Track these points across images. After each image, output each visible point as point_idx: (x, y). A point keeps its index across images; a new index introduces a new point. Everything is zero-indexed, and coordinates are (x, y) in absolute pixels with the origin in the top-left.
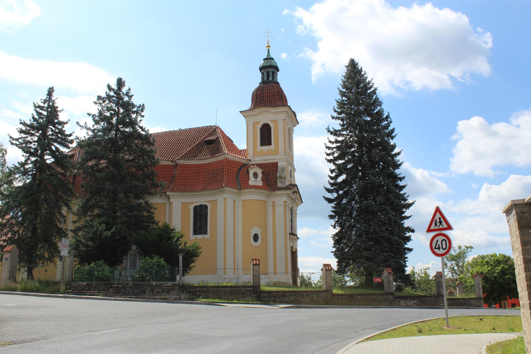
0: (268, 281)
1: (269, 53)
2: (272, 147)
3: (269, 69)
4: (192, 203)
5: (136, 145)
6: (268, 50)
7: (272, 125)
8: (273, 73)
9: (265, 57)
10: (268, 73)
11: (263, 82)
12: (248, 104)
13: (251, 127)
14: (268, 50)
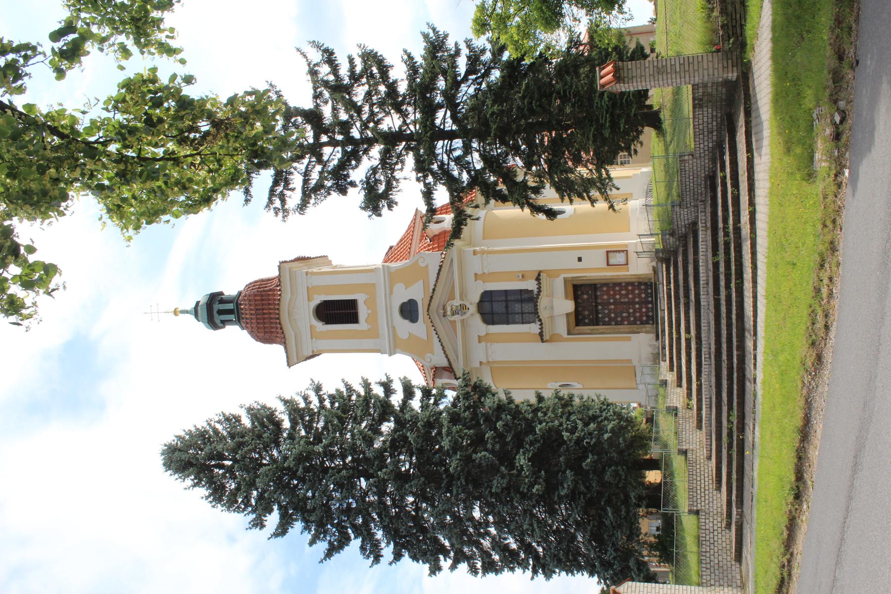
0: (647, 370)
1: (187, 312)
2: (361, 298)
3: (216, 311)
4: (393, 330)
5: (132, 206)
6: (183, 312)
7: (318, 299)
8: (222, 301)
10: (221, 312)
11: (239, 321)
12: (277, 350)
14: (183, 312)
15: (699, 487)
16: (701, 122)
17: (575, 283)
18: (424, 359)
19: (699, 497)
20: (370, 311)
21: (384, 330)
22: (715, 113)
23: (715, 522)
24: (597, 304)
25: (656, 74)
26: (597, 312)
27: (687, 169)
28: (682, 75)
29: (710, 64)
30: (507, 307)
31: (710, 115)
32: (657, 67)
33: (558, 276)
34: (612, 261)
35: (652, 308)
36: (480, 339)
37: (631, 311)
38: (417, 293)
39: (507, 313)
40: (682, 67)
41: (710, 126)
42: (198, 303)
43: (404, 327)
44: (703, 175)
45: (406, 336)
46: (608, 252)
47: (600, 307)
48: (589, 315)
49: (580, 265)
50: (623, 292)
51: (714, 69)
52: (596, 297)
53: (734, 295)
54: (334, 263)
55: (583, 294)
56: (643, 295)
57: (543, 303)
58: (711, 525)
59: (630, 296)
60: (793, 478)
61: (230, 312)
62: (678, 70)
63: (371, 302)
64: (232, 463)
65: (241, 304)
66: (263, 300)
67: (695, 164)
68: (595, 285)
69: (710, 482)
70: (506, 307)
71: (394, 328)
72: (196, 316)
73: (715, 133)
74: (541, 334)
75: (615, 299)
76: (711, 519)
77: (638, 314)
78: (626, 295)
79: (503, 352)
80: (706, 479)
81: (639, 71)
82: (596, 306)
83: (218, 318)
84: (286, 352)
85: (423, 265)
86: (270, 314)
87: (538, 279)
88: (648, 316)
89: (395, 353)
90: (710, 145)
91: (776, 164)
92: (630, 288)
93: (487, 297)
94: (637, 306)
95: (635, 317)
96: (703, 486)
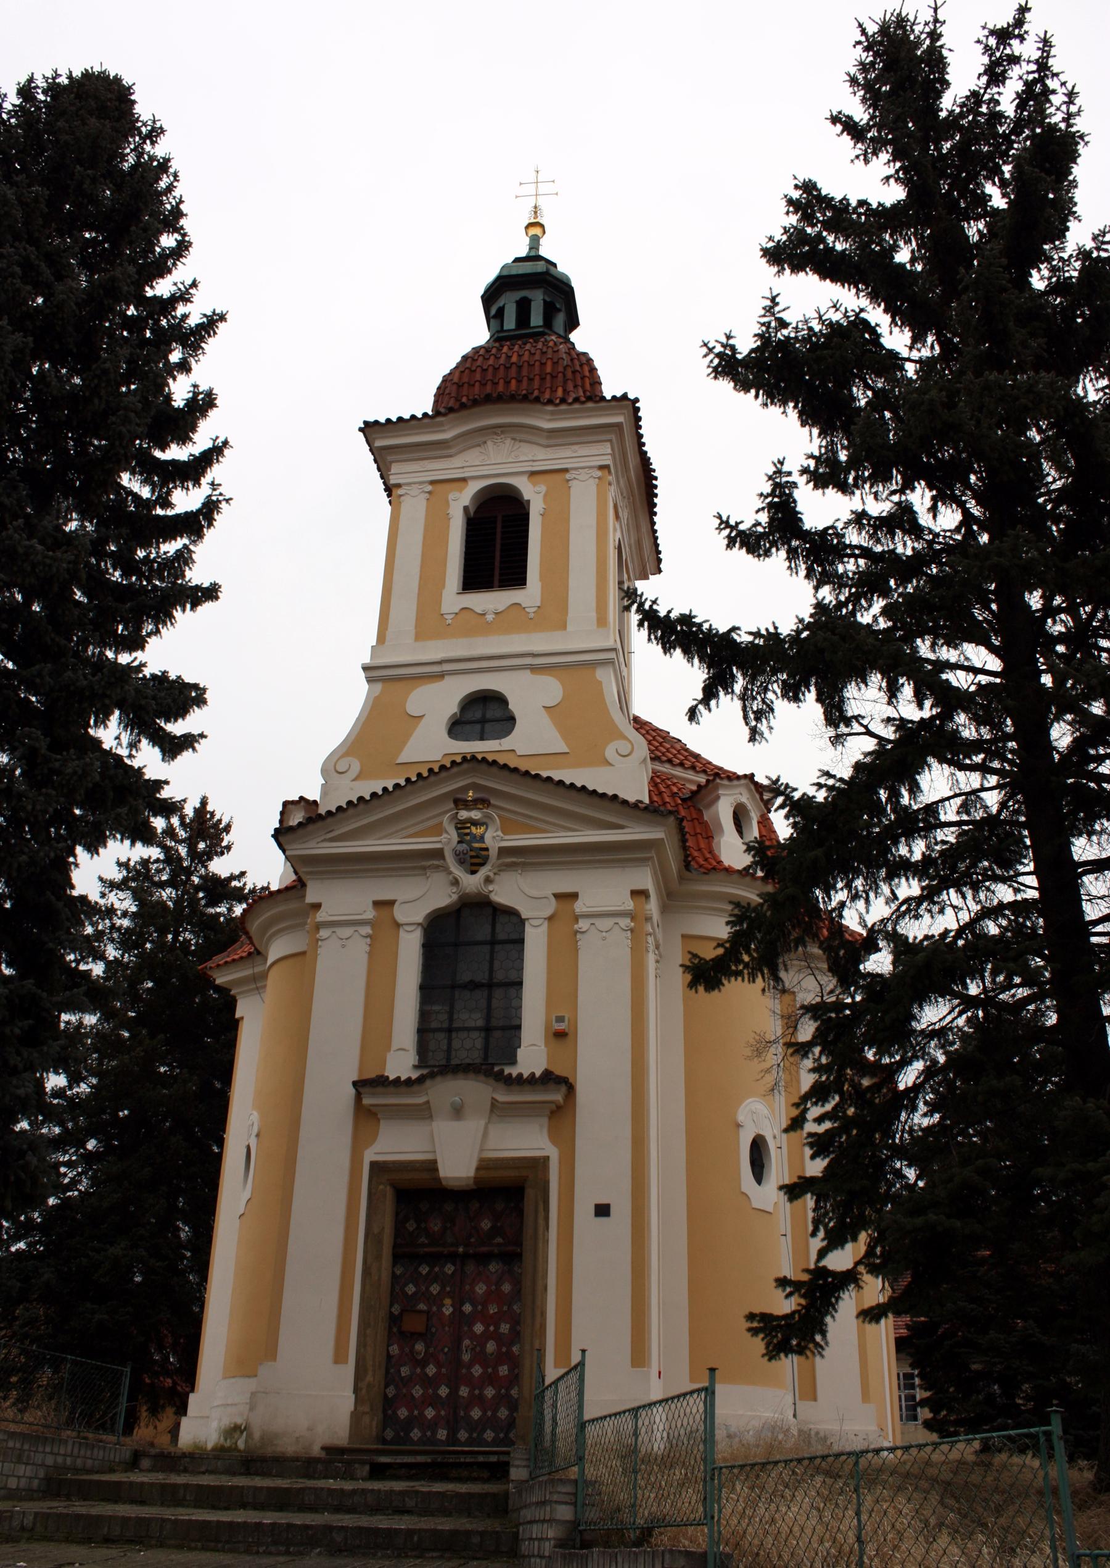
4: (433, 673)
7: (533, 494)
10: (524, 307)
17: (530, 1193)
20: (490, 617)
26: (433, 1259)
30: (473, 986)
33: (555, 1136)
35: (482, 1442)
37: (431, 1370)
38: (533, 738)
39: (453, 987)
43: (440, 701)
45: (412, 708)
47: (449, 1269)
50: (491, 1347)
52: (484, 1259)
57: (474, 1091)
59: (477, 1370)
60: (848, 1450)
66: (543, 379)
70: (470, 968)
71: (441, 676)
74: (380, 1082)
75: (471, 1320)
77: (417, 1392)
82: (452, 1257)
83: (509, 302)
85: (610, 753)
87: (549, 1079)
88: (409, 1424)
89: (369, 680)
92: (503, 1370)
93: (500, 928)
94: (464, 1392)
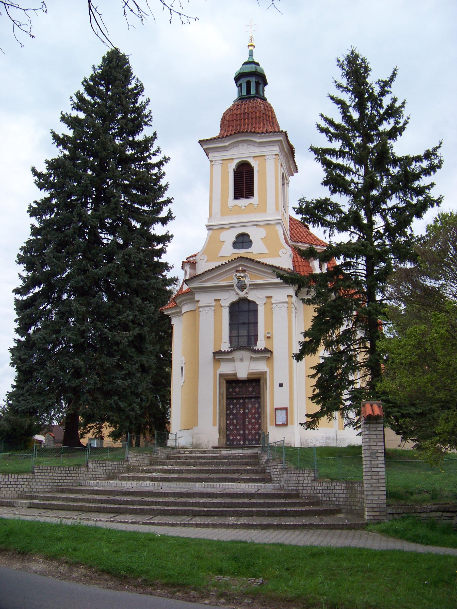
2: (255, 200)
3: (251, 80)
4: (227, 227)
7: (254, 163)
9: (246, 61)
11: (241, 98)
12: (216, 131)
13: (218, 169)
15: (54, 474)
16: (336, 488)
18: (203, 254)
19: (46, 474)
21: (227, 220)
22: (342, 499)
23: (24, 486)
24: (243, 398)
25: (371, 451)
27: (305, 475)
28: (369, 473)
29: (376, 497)
30: (244, 324)
31: (340, 495)
32: (377, 452)
34: (278, 412)
35: (240, 444)
36: (217, 300)
37: (238, 427)
39: (249, 324)
40: (376, 473)
41: (333, 495)
42: (258, 64)
43: (230, 236)
44: (300, 488)
46: (286, 409)
48: (235, 392)
49: (276, 385)
51: (372, 500)
52: (250, 398)
53: (132, 507)
54: (291, 178)
55: (253, 387)
56: (250, 437)
57: (246, 354)
58: (22, 483)
61: (249, 91)
62: (373, 470)
63: (250, 209)
64: (112, 95)
65: (254, 100)
67: (307, 482)
68: (259, 397)
69: (59, 484)
71: (230, 228)
72: (246, 63)
73: (328, 499)
76: (26, 483)
77: (235, 432)
78: (250, 423)
79: (206, 319)
80: (62, 481)
81: (375, 437)
82: (242, 398)
84: (211, 139)
85: (280, 253)
86: (244, 125)
87: (266, 351)
88: (233, 440)
90: (320, 495)
91: (254, 547)
95: (232, 430)
96: (56, 478)
